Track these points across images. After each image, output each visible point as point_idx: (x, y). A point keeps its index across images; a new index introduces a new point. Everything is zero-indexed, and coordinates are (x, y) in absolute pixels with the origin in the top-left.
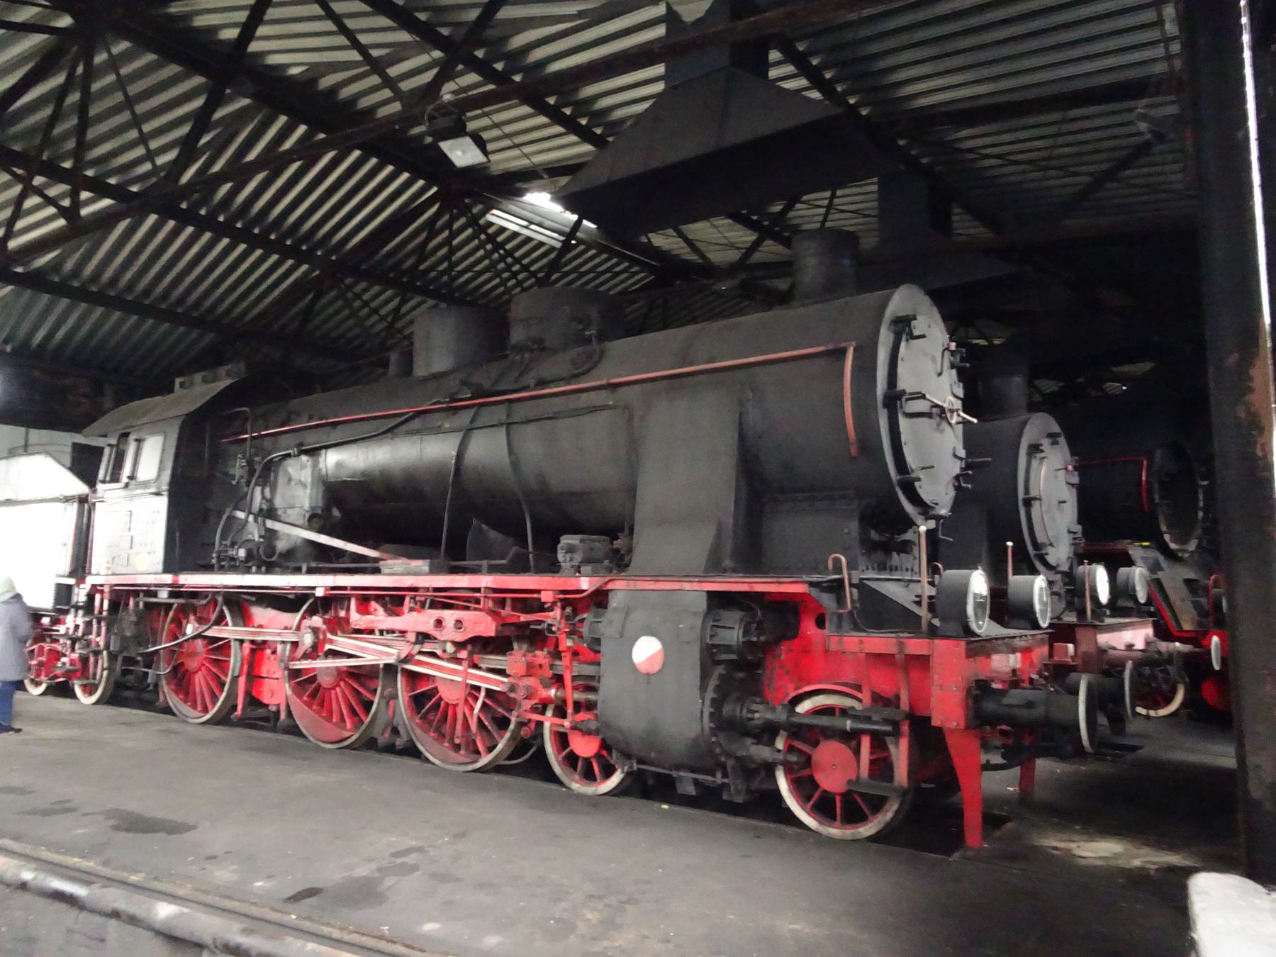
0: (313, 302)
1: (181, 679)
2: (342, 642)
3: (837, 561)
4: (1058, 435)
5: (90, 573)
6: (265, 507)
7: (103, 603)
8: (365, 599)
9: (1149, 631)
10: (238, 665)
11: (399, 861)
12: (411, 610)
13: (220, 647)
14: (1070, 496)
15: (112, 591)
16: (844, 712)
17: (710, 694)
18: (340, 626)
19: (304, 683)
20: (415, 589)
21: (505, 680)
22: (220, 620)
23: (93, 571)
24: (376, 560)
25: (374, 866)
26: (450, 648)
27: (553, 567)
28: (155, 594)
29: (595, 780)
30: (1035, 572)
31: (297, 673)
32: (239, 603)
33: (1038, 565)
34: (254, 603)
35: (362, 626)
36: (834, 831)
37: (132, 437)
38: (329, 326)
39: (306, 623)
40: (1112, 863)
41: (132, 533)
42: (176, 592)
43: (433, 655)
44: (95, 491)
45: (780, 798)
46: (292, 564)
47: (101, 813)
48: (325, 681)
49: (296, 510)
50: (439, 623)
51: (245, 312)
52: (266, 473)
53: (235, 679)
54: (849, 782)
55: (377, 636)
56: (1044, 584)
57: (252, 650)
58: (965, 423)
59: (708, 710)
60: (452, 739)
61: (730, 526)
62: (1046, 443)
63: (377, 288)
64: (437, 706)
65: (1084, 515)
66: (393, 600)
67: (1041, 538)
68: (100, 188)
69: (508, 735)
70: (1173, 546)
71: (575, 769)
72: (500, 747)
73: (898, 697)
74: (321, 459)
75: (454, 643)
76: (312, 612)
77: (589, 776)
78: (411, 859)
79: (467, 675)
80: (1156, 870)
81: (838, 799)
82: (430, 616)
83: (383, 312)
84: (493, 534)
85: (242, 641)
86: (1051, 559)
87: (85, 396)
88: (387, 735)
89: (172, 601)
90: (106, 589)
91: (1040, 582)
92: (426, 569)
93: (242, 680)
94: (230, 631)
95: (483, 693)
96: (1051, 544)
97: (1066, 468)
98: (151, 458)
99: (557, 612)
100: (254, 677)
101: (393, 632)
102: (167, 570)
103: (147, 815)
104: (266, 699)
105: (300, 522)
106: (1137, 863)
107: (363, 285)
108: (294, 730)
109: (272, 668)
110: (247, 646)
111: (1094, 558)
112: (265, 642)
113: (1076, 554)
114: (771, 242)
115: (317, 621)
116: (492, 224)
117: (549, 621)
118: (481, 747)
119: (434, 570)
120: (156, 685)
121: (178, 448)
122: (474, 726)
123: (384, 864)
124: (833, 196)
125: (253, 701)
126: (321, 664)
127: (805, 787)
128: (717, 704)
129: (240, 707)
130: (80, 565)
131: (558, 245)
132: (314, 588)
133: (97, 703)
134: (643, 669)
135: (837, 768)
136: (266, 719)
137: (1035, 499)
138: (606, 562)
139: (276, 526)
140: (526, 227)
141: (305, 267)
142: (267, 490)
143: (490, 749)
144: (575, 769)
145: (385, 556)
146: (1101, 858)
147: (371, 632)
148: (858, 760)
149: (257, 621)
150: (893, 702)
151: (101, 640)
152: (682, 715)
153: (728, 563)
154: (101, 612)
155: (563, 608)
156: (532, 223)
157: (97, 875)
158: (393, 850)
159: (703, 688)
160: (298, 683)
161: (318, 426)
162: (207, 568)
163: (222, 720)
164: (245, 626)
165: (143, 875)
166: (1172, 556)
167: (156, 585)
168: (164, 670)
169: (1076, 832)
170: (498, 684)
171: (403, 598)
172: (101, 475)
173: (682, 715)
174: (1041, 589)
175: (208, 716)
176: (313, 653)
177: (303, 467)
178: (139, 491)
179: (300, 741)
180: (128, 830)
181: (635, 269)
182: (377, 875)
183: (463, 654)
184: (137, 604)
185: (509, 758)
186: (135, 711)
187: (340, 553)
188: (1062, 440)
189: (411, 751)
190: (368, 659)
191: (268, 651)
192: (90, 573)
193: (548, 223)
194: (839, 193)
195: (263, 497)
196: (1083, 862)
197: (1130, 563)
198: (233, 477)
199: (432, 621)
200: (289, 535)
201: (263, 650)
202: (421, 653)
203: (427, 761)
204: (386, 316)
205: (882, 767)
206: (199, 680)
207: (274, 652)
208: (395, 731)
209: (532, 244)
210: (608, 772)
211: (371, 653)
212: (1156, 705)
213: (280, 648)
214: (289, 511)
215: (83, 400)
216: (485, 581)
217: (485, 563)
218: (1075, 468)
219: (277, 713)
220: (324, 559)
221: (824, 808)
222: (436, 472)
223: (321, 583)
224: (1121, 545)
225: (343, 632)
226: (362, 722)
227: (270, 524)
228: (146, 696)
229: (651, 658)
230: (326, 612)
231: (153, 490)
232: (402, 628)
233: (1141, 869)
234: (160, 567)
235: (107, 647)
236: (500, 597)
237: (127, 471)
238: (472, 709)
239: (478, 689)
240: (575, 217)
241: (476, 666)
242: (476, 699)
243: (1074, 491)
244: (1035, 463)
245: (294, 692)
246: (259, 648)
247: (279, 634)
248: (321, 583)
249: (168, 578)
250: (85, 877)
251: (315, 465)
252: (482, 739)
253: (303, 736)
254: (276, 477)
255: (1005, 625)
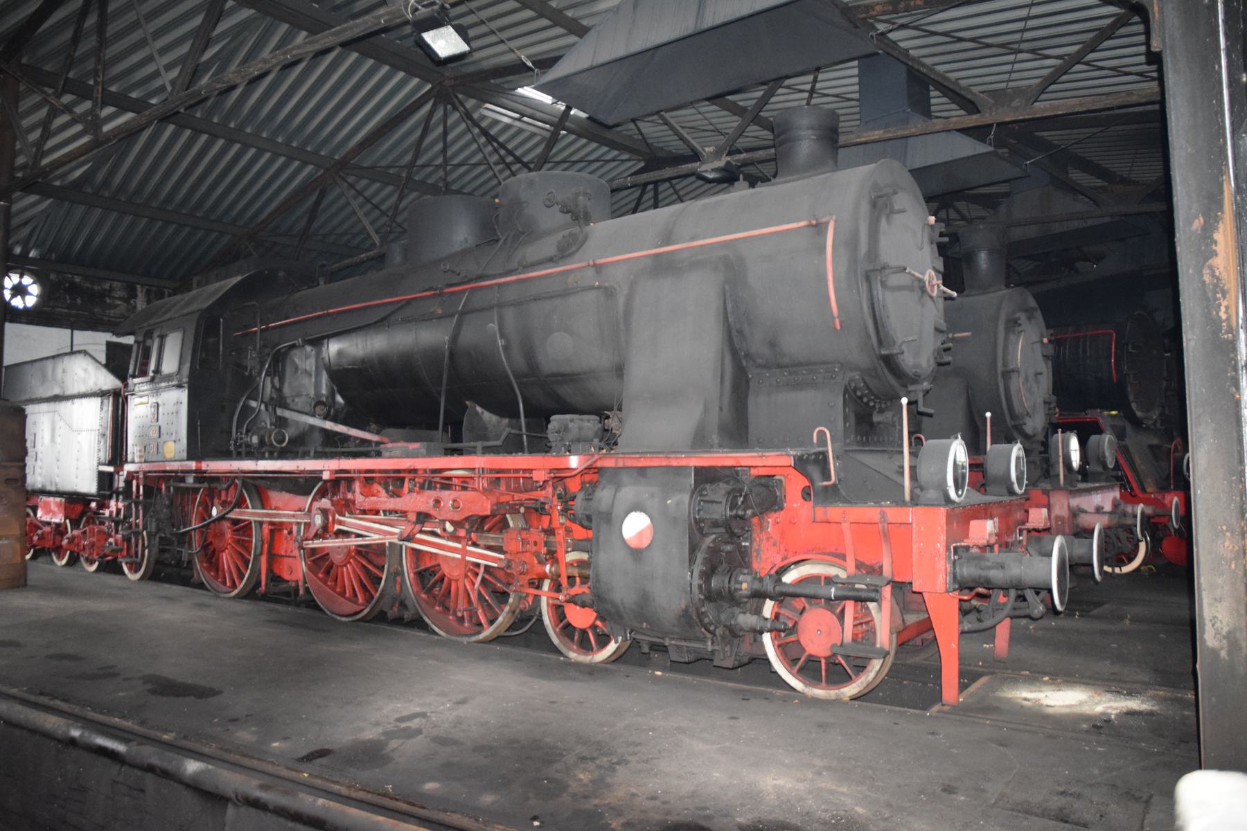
0: (318, 203)
1: (211, 557)
2: (350, 522)
3: (822, 434)
4: (1033, 309)
5: (126, 461)
6: (274, 396)
7: (138, 488)
8: (369, 479)
9: (1116, 494)
10: (259, 545)
11: (403, 725)
12: (411, 491)
13: (243, 528)
14: (1045, 369)
15: (146, 477)
16: (829, 580)
17: (698, 567)
18: (347, 507)
19: (319, 560)
20: (415, 471)
21: (502, 556)
22: (240, 503)
23: (129, 459)
24: (378, 443)
25: (380, 729)
26: (450, 528)
27: (540, 445)
28: (183, 480)
29: (592, 649)
30: (1010, 440)
31: (314, 551)
32: (259, 487)
33: (1015, 434)
34: (270, 488)
35: (367, 507)
36: (819, 692)
37: (156, 334)
38: (335, 222)
39: (317, 505)
40: (1075, 710)
41: (160, 423)
42: (201, 476)
43: (434, 534)
44: (126, 385)
45: (767, 661)
46: (301, 450)
47: (140, 678)
48: (337, 558)
49: (304, 398)
50: (437, 502)
51: (256, 215)
52: (278, 363)
53: (257, 558)
54: (833, 646)
55: (381, 516)
56: (1022, 453)
57: (272, 532)
58: (948, 298)
59: (697, 581)
60: (455, 613)
61: (454, 251)
62: (1022, 317)
63: (377, 185)
64: (442, 579)
65: (1059, 387)
66: (395, 481)
67: (1018, 409)
68: (123, 103)
69: (507, 608)
70: (1139, 414)
71: (572, 639)
72: (500, 619)
73: (881, 567)
74: (324, 349)
75: (452, 522)
76: (322, 493)
77: (585, 646)
78: (414, 724)
79: (465, 553)
80: (1117, 715)
81: (823, 661)
82: (429, 497)
83: (383, 207)
84: (487, 416)
85: (261, 523)
86: (1028, 429)
87: (119, 299)
88: (395, 609)
89: (197, 485)
90: (141, 476)
91: (1016, 450)
92: (424, 451)
93: (264, 559)
94: (250, 513)
95: (482, 570)
96: (1028, 414)
97: (1041, 341)
98: (171, 356)
99: (550, 490)
100: (273, 558)
101: (396, 512)
102: (190, 457)
103: (180, 680)
104: (286, 576)
105: (307, 409)
106: (1099, 709)
107: (364, 182)
108: (311, 604)
109: (287, 546)
110: (266, 528)
111: (1067, 428)
112: (281, 524)
113: (1051, 424)
114: (756, 128)
115: (325, 503)
116: (484, 117)
117: (542, 500)
118: (483, 620)
119: (430, 453)
120: (190, 562)
121: (195, 345)
122: (474, 597)
123: (390, 728)
124: (815, 81)
125: (275, 578)
126: (331, 543)
127: (790, 653)
128: (707, 575)
129: (263, 583)
130: (118, 453)
131: (548, 135)
132: (321, 472)
133: (142, 579)
134: (634, 544)
135: (821, 633)
136: (287, 594)
137: (1013, 371)
138: (596, 441)
139: (287, 414)
140: (519, 120)
141: (310, 168)
142: (276, 380)
143: (492, 622)
144: (572, 639)
145: (385, 440)
146: (1067, 706)
147: (377, 513)
148: (842, 625)
149: (274, 504)
150: (876, 571)
151: (140, 521)
152: (673, 586)
153: (715, 438)
154: (138, 497)
155: (555, 488)
156: (523, 115)
157: (135, 734)
158: (397, 716)
159: (692, 561)
160: (313, 561)
161: (319, 317)
162: (226, 455)
163: (250, 594)
164: (264, 508)
165: (173, 734)
166: (1137, 423)
167: (182, 472)
168: (196, 547)
169: (1046, 683)
170: (492, 559)
171: (402, 479)
172: (131, 371)
173: (673, 586)
174: (1018, 458)
175: (236, 591)
176: (324, 532)
177: (307, 357)
178: (163, 384)
179: (317, 614)
180: (162, 694)
181: (625, 156)
182: (383, 738)
183: (462, 533)
184: (168, 488)
185: (510, 629)
186: (174, 587)
187: (345, 438)
188: (1039, 314)
189: (418, 623)
190: (374, 539)
191: (285, 532)
192: (126, 461)
193: (539, 115)
194: (821, 77)
195: (273, 386)
196: (1050, 711)
197: (1100, 431)
198: (245, 368)
199: (431, 502)
200: (297, 422)
201: (281, 530)
202: (421, 532)
203: (434, 633)
204: (388, 210)
205: (865, 628)
206: (226, 558)
207: (290, 533)
208: (403, 605)
209: (525, 135)
210: (603, 641)
211: (377, 532)
212: (1121, 563)
213: (295, 528)
214: (297, 400)
215: (118, 302)
216: (480, 461)
217: (479, 445)
218: (1050, 341)
219: (297, 590)
220: (332, 445)
221: (810, 669)
222: (432, 356)
223: (326, 467)
224: (1091, 414)
225: (351, 513)
226: (372, 597)
227: (279, 412)
228: (183, 573)
229: (640, 534)
230: (334, 494)
231: (175, 383)
232: (404, 509)
233: (1103, 714)
234: (185, 455)
235: (145, 528)
236: (497, 477)
237: (152, 366)
238: (474, 584)
239: (478, 565)
240: (561, 107)
241: (475, 544)
242: (476, 574)
243: (1050, 363)
244: (1012, 337)
245: (309, 568)
246: (277, 528)
247: (293, 516)
248: (326, 467)
249: (193, 465)
250: (126, 735)
251: (318, 354)
252: (484, 611)
253: (320, 609)
254: (284, 367)
255: (985, 493)
